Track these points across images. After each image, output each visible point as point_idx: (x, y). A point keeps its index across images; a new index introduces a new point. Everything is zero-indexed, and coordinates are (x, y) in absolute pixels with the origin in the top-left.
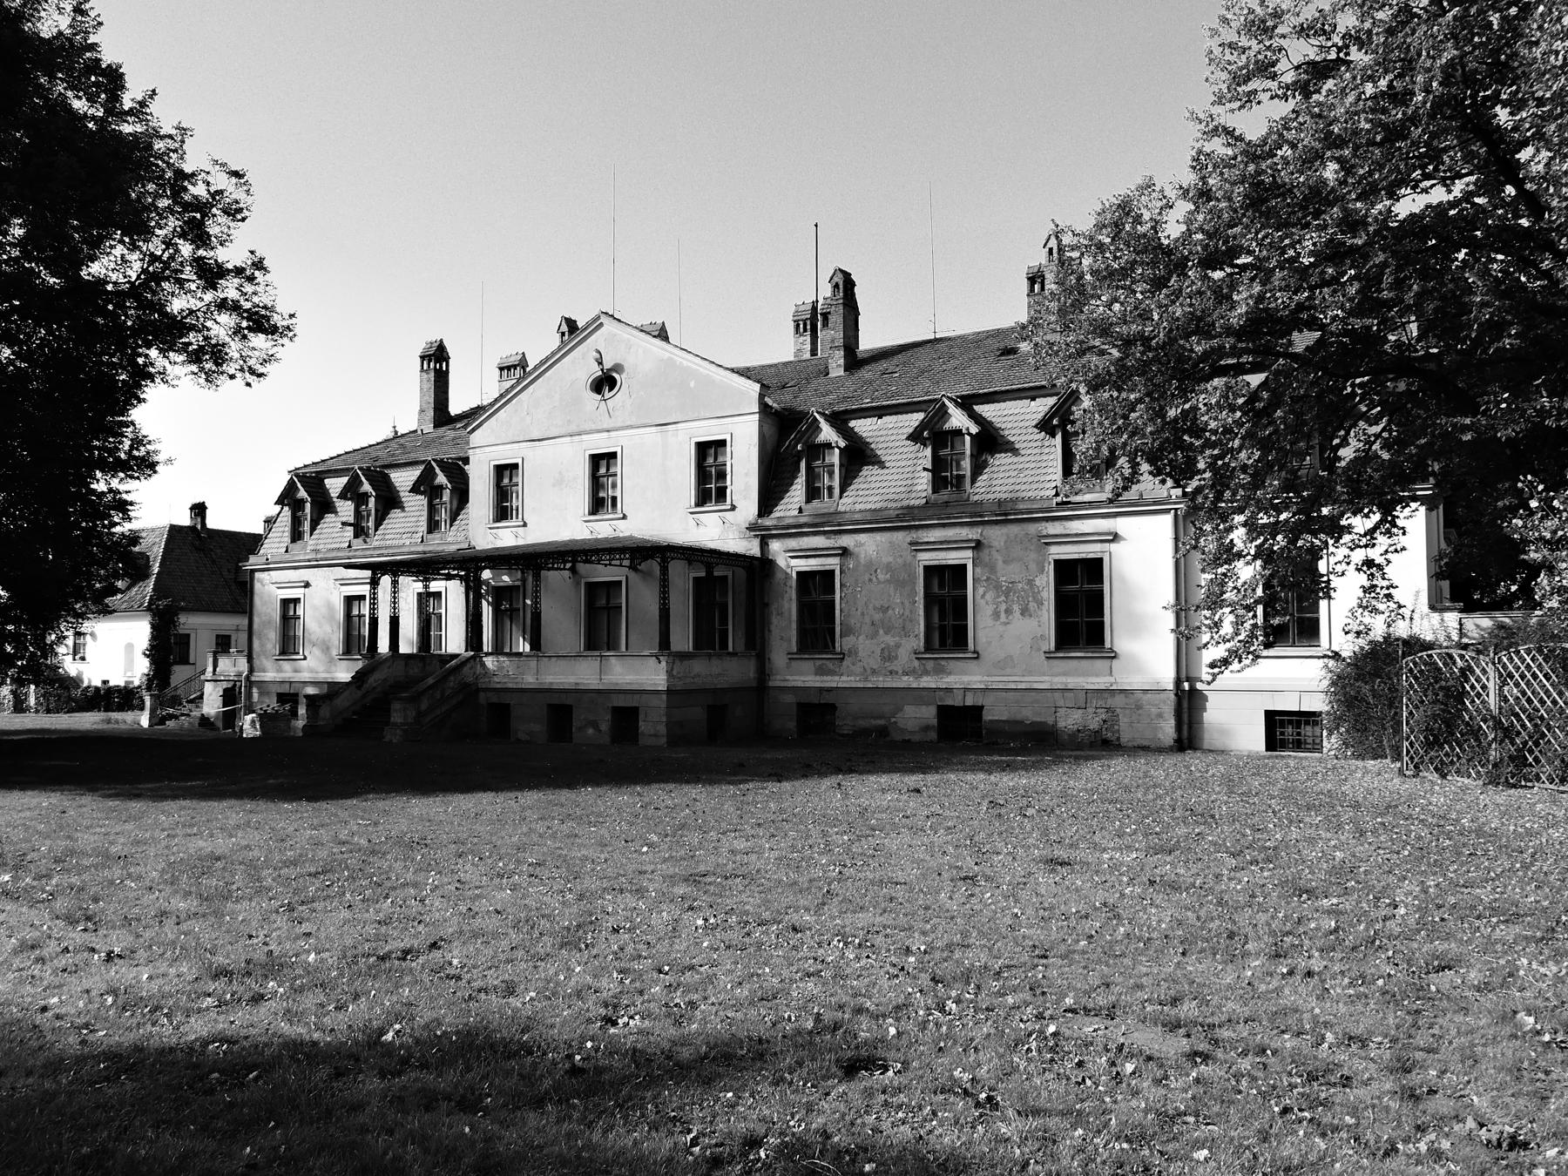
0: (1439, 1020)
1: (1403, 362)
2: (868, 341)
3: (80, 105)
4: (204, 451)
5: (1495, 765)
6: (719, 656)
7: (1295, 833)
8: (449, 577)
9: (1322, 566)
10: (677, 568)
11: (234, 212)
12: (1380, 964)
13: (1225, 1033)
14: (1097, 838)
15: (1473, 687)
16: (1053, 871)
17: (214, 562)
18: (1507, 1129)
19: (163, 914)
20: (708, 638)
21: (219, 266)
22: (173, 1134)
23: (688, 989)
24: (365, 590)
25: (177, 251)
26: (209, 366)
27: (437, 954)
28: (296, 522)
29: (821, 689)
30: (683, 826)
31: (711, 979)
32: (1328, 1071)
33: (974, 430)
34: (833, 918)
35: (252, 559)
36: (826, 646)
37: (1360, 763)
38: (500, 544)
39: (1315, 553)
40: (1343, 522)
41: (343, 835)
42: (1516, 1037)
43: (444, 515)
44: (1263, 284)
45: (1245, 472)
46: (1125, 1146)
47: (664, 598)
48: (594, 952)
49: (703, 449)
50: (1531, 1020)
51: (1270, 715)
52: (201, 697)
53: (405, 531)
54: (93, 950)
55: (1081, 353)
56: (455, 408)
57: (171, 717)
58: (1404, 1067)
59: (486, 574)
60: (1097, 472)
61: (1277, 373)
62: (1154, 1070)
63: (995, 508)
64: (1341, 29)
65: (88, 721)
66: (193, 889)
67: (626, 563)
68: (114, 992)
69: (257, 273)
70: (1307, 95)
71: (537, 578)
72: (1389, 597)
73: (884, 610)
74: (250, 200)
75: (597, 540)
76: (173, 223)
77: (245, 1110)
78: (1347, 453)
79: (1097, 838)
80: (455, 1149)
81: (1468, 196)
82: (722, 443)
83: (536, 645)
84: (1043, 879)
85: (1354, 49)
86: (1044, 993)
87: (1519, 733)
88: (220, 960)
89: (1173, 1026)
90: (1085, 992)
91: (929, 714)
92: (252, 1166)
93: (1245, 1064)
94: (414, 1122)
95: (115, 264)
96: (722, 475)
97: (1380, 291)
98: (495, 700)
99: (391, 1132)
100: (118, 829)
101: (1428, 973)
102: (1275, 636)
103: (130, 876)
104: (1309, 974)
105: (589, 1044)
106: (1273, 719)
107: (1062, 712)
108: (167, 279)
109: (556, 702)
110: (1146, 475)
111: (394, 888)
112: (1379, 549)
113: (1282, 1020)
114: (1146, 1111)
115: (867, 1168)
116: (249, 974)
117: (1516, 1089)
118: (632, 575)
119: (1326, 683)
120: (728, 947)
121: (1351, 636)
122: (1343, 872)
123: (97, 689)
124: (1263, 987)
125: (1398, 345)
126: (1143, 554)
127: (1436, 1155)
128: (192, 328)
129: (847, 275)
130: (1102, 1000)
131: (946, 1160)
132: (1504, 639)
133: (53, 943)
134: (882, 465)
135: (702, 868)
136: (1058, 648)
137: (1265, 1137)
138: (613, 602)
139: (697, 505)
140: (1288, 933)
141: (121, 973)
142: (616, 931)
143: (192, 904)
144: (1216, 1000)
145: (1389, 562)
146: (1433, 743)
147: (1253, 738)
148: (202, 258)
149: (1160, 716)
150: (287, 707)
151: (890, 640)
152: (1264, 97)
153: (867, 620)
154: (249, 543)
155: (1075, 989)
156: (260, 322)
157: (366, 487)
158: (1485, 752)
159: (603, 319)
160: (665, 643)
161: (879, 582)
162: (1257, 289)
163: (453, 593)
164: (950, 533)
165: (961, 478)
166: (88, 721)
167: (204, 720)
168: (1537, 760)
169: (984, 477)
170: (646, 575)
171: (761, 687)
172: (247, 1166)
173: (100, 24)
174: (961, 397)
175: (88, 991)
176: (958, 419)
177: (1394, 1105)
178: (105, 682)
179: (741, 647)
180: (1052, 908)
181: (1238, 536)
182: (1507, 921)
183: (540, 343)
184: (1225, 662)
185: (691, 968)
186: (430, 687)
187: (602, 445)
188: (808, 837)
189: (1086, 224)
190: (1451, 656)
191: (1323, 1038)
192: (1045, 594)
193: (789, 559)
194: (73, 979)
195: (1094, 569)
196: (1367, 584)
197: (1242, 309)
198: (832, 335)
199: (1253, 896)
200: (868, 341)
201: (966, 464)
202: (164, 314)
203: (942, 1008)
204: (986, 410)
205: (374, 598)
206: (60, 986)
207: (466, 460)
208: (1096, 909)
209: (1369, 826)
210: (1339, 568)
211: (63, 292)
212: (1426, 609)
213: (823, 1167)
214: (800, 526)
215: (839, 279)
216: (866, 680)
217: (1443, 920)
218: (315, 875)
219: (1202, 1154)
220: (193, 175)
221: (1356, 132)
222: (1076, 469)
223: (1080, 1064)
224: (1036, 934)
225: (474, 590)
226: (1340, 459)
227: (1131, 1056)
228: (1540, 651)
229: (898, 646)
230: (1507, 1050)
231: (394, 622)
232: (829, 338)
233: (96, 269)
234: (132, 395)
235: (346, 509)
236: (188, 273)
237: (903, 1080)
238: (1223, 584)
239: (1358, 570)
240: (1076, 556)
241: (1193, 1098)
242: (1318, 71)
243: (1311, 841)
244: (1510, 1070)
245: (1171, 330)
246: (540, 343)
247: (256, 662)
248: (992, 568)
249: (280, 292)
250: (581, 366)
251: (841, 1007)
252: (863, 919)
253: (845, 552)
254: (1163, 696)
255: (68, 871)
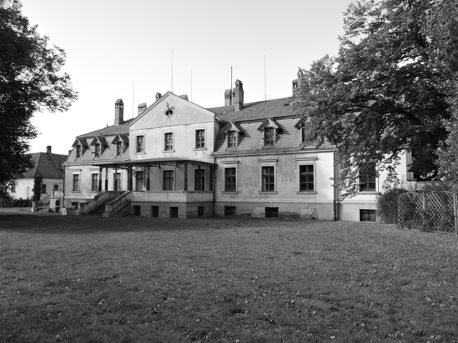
0: (404, 299)
1: (400, 110)
2: (247, 101)
3: (15, 29)
4: (50, 131)
5: (424, 226)
6: (202, 192)
7: (366, 245)
8: (123, 169)
9: (376, 168)
10: (189, 166)
11: (60, 62)
12: (388, 283)
13: (342, 303)
14: (309, 246)
15: (418, 203)
16: (295, 256)
17: (53, 163)
18: (420, 330)
19: (35, 267)
20: (199, 187)
21: (56, 77)
22: (36, 331)
23: (189, 289)
24: (98, 172)
25: (44, 72)
26: (52, 106)
27: (116, 279)
28: (78, 152)
29: (231, 202)
30: (189, 242)
31: (195, 287)
32: (370, 313)
33: (277, 127)
34: (232, 269)
35: (65, 163)
36: (233, 190)
37: (386, 225)
38: (138, 159)
39: (374, 165)
40: (383, 155)
41: (90, 244)
42: (425, 304)
43: (121, 150)
44: (360, 87)
45: (355, 141)
46: (311, 335)
47: (186, 175)
48: (162, 279)
49: (198, 132)
50: (429, 299)
51: (361, 211)
52: (49, 203)
53: (110, 155)
54: (14, 278)
55: (307, 106)
56: (125, 119)
57: (40, 209)
58: (392, 312)
59: (134, 168)
60: (311, 140)
61: (364, 112)
62: (321, 313)
63: (283, 150)
64: (382, 14)
65: (15, 211)
66: (45, 260)
67: (175, 165)
68: (20, 290)
69: (67, 80)
70: (372, 32)
71: (149, 169)
72: (395, 177)
73: (250, 179)
74: (65, 58)
75: (166, 158)
76: (42, 64)
77: (57, 324)
78: (383, 136)
79: (309, 246)
80: (118, 335)
81: (419, 62)
82: (203, 130)
83: (148, 189)
84: (293, 258)
85: (386, 19)
86: (291, 291)
87: (431, 217)
88: (52, 281)
89: (327, 300)
90: (303, 291)
91: (263, 210)
92: (58, 340)
93: (347, 311)
94: (107, 327)
95: (24, 76)
96: (203, 140)
97: (392, 89)
98: (136, 205)
99: (99, 331)
100: (23, 242)
101: (401, 285)
102: (363, 187)
103: (26, 256)
104: (367, 286)
105: (159, 305)
106: (362, 212)
107: (301, 209)
108: (40, 80)
109: (154, 205)
110: (326, 141)
111: (103, 260)
112: (393, 164)
113: (358, 299)
114: (318, 325)
115: (237, 341)
116: (60, 285)
117: (423, 319)
118: (177, 168)
119: (377, 202)
120: (201, 277)
121: (384, 189)
122: (379, 256)
123: (18, 200)
124: (354, 290)
125: (398, 105)
126: (325, 163)
127: (399, 337)
128: (47, 95)
129: (240, 82)
130: (308, 293)
131: (260, 339)
132: (427, 190)
133: (3, 275)
134: (249, 137)
135: (194, 254)
136: (300, 191)
137: (351, 332)
138: (171, 176)
139: (196, 148)
140: (362, 274)
141: (22, 284)
142: (168, 273)
143: (45, 264)
144: (340, 293)
145: (396, 167)
146: (407, 218)
147: (356, 217)
148: (50, 75)
149: (329, 211)
150: (75, 206)
151: (252, 188)
152: (360, 32)
153: (245, 182)
154: (64, 158)
155: (300, 290)
156: (67, 94)
157: (99, 142)
158: (422, 222)
159: (169, 94)
160: (186, 189)
161: (249, 171)
162: (358, 88)
163: (124, 173)
164: (269, 157)
165: (272, 141)
166: (15, 211)
167: (50, 210)
168: (436, 224)
169: (279, 141)
170: (181, 168)
171: (214, 202)
172: (57, 340)
173: (22, 5)
174: (273, 118)
175: (12, 290)
176: (272, 124)
177: (389, 323)
178: (21, 198)
179: (208, 190)
180: (295, 267)
181: (352, 159)
182: (425, 271)
183: (150, 100)
184: (347, 195)
185: (190, 283)
186: (117, 201)
187: (168, 130)
188: (226, 245)
189: (308, 68)
190: (412, 194)
191: (370, 304)
192: (296, 175)
193: (222, 164)
194: (8, 286)
195: (311, 167)
196: (389, 173)
197: (353, 94)
198: (235, 99)
199: (353, 263)
200: (247, 101)
201: (274, 137)
202: (39, 91)
203: (261, 295)
204: (280, 122)
205: (101, 175)
206: (4, 288)
207: (128, 134)
208: (308, 267)
209: (388, 243)
210: (382, 169)
211: (9, 84)
212: (406, 181)
213: (224, 341)
214: (226, 155)
215: (238, 83)
216: (244, 199)
217: (406, 270)
218: (81, 256)
219: (333, 337)
220: (49, 50)
221: (386, 43)
222: (305, 139)
223: (300, 311)
224: (290, 274)
225: (130, 172)
226: (381, 137)
227: (315, 309)
228: (437, 193)
229: (254, 190)
230: (422, 308)
231: (107, 182)
232: (235, 100)
233: (19, 78)
234: (29, 114)
235: (93, 148)
236: (47, 79)
237: (248, 316)
238: (347, 172)
239: (387, 169)
240: (306, 164)
241: (332, 321)
242: (375, 26)
243: (371, 247)
244: (422, 313)
245: (333, 100)
246: (150, 100)
247: (66, 194)
248: (281, 167)
249: (74, 85)
250: (162, 107)
251: (232, 295)
252: (241, 269)
253: (239, 162)
254: (330, 205)
255: (8, 254)
